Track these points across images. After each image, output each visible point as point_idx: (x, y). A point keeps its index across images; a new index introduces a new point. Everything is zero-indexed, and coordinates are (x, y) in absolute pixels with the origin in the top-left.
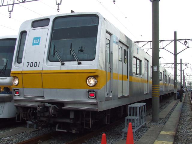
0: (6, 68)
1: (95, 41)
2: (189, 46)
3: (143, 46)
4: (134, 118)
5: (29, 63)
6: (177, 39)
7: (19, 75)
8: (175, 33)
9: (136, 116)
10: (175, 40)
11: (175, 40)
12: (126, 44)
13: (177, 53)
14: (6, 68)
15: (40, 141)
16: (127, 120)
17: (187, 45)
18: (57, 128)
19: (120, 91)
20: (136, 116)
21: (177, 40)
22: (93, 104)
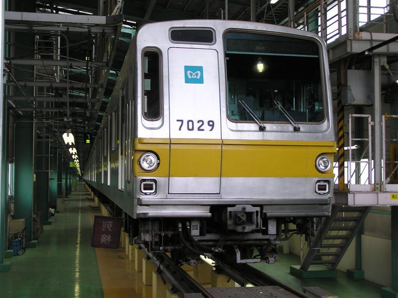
5: (182, 121)
7: (161, 146)
22: (201, 205)
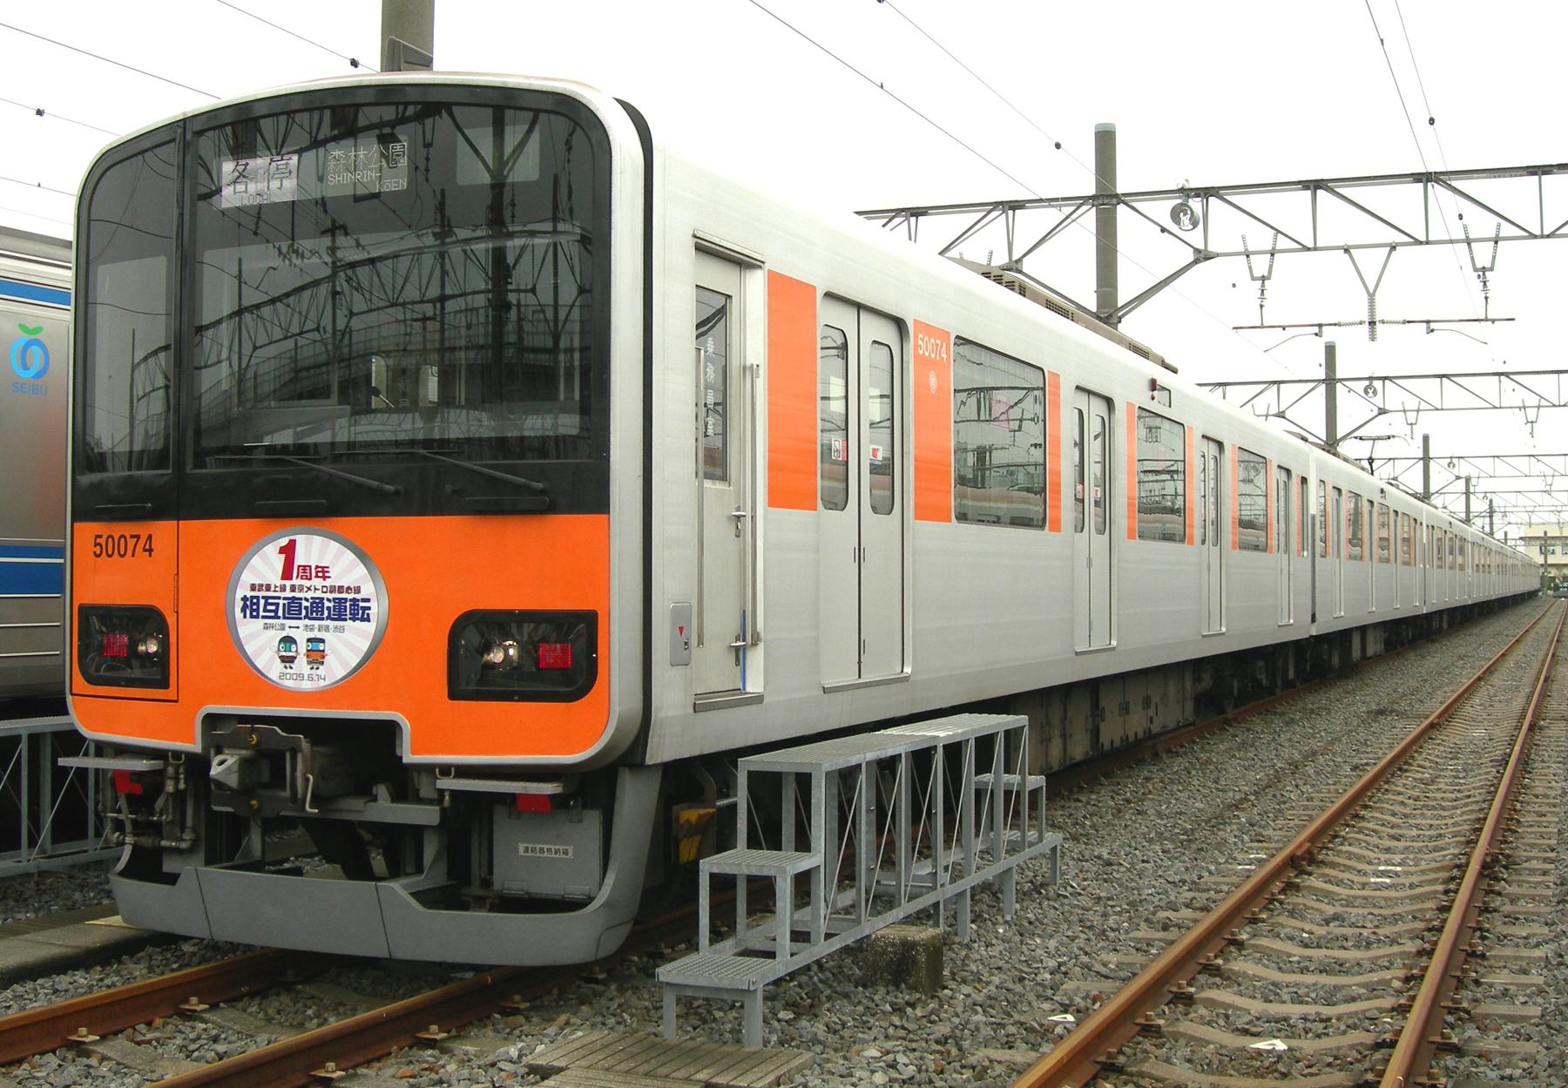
0: (499, 323)
1: (371, 91)
2: (1212, 248)
3: (1405, 322)
4: (783, 865)
6: (1119, 191)
8: (1105, 141)
9: (803, 843)
10: (1106, 200)
11: (1106, 200)
12: (526, 127)
13: (1120, 304)
14: (499, 323)
15: (517, 998)
16: (723, 884)
17: (1196, 238)
18: (283, 794)
19: (1081, 631)
20: (803, 843)
21: (1120, 199)
